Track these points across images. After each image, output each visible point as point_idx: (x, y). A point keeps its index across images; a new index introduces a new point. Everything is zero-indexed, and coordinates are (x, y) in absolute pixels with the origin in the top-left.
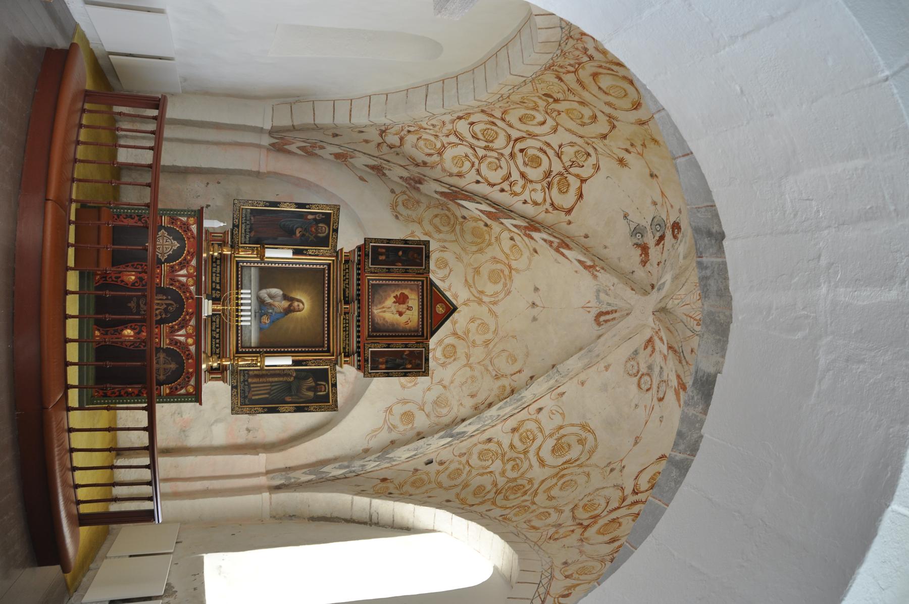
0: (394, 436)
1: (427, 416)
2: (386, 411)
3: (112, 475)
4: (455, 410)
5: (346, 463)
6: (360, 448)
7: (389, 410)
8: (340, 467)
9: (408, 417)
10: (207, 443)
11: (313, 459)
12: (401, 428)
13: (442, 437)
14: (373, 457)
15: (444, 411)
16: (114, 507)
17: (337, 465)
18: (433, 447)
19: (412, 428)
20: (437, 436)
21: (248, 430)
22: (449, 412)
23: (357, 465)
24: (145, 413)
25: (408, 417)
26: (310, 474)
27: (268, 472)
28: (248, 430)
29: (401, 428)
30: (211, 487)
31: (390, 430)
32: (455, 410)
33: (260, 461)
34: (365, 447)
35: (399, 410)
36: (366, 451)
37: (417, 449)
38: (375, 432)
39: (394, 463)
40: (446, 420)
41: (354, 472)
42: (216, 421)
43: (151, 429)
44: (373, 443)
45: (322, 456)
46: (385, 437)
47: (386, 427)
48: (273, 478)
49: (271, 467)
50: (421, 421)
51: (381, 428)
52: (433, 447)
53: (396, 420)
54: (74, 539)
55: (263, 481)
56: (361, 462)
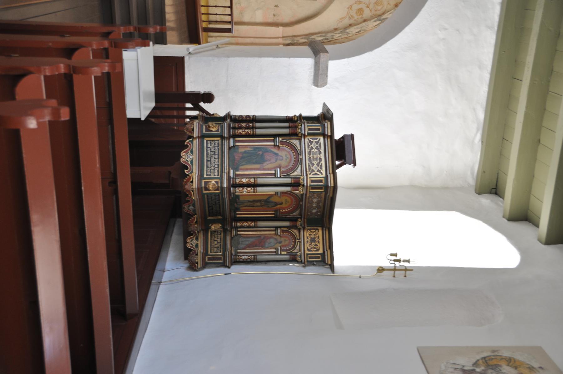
0: (352, 21)
1: (371, 10)
2: (348, 8)
3: (208, 10)
4: (385, 7)
5: (324, 34)
6: (332, 28)
7: (350, 7)
8: (321, 36)
9: (360, 11)
10: (253, 20)
11: (307, 32)
12: (356, 17)
13: (375, 21)
14: (338, 32)
15: (379, 8)
16: (211, 26)
17: (319, 35)
18: (370, 26)
19: (362, 18)
20: (372, 20)
21: (274, 15)
22: (382, 8)
23: (329, 36)
24: (229, 9)
25: (360, 11)
26: (305, 39)
27: (283, 37)
28: (274, 15)
29: (356, 17)
30: (421, 257)
31: (350, 18)
32: (385, 7)
33: (280, 31)
34: (336, 27)
35: (356, 7)
36: (336, 29)
37: (361, 28)
38: (342, 19)
39: (349, 35)
40: (379, 13)
41: (328, 39)
42: (258, 9)
43: (231, 15)
44: (340, 25)
45: (312, 31)
46: (347, 22)
47: (348, 16)
48: (285, 40)
49: (285, 35)
50: (367, 13)
51: (344, 18)
52: (370, 26)
53: (353, 13)
54: (202, 35)
55: (280, 40)
56: (332, 34)
